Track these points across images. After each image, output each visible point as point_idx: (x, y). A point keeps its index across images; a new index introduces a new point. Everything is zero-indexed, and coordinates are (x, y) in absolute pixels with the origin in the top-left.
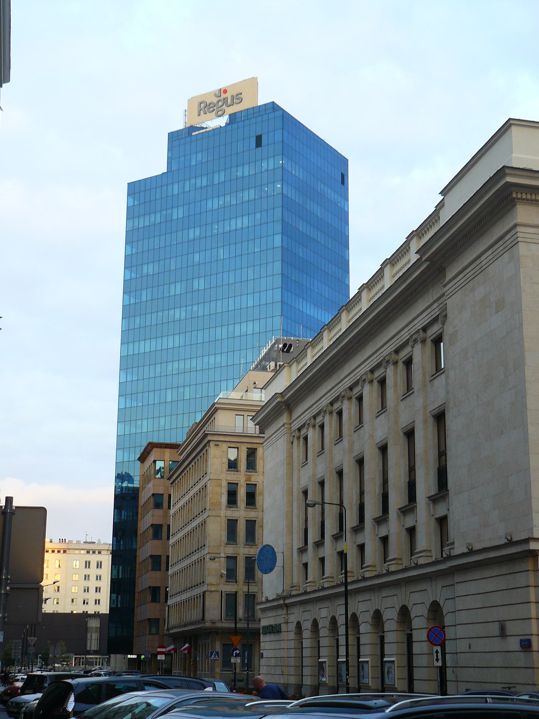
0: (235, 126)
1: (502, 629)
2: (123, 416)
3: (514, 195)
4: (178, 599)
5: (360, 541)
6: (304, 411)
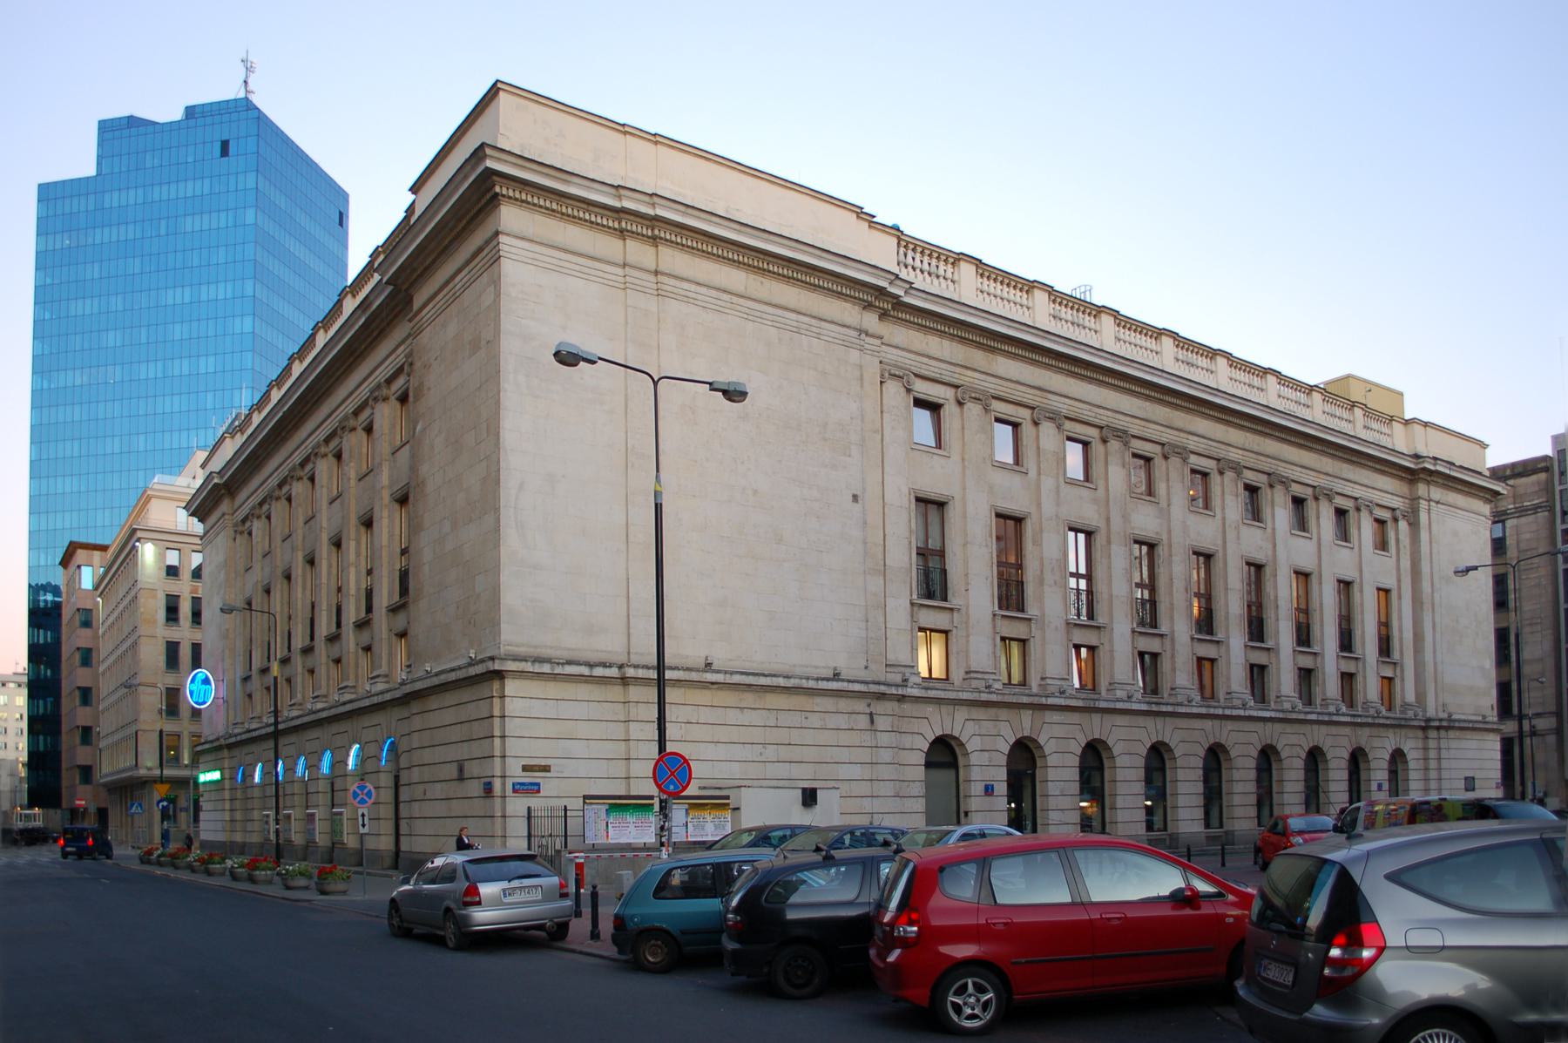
0: (192, 122)
1: (461, 770)
2: (39, 505)
3: (497, 189)
4: (110, 740)
5: (309, 665)
6: (248, 496)
